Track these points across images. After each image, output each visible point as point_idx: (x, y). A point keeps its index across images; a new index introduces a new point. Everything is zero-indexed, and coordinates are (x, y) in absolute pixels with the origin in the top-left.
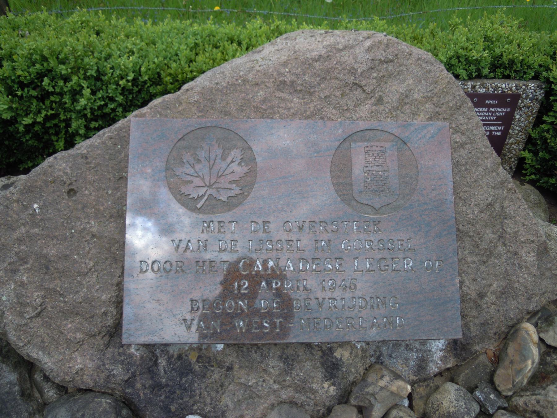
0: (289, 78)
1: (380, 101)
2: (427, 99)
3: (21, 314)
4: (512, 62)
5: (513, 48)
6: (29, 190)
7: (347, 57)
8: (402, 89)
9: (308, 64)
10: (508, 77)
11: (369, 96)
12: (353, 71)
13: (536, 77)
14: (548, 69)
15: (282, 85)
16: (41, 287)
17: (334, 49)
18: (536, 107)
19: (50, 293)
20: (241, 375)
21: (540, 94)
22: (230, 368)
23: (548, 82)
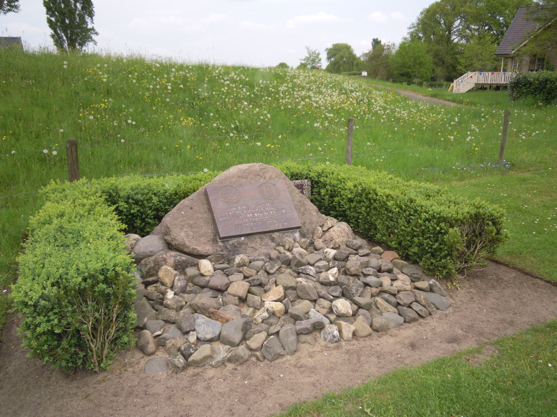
0: (240, 175)
1: (265, 178)
2: (276, 177)
3: (188, 238)
4: (297, 174)
5: (296, 169)
6: (179, 209)
7: (253, 168)
8: (269, 175)
9: (244, 171)
10: (297, 179)
11: (262, 177)
12: (256, 171)
13: (306, 178)
14: (309, 174)
15: (239, 177)
16: (191, 231)
17: (250, 167)
18: (310, 188)
19: (194, 232)
20: (250, 245)
21: (310, 183)
22: (247, 244)
23: (311, 178)
